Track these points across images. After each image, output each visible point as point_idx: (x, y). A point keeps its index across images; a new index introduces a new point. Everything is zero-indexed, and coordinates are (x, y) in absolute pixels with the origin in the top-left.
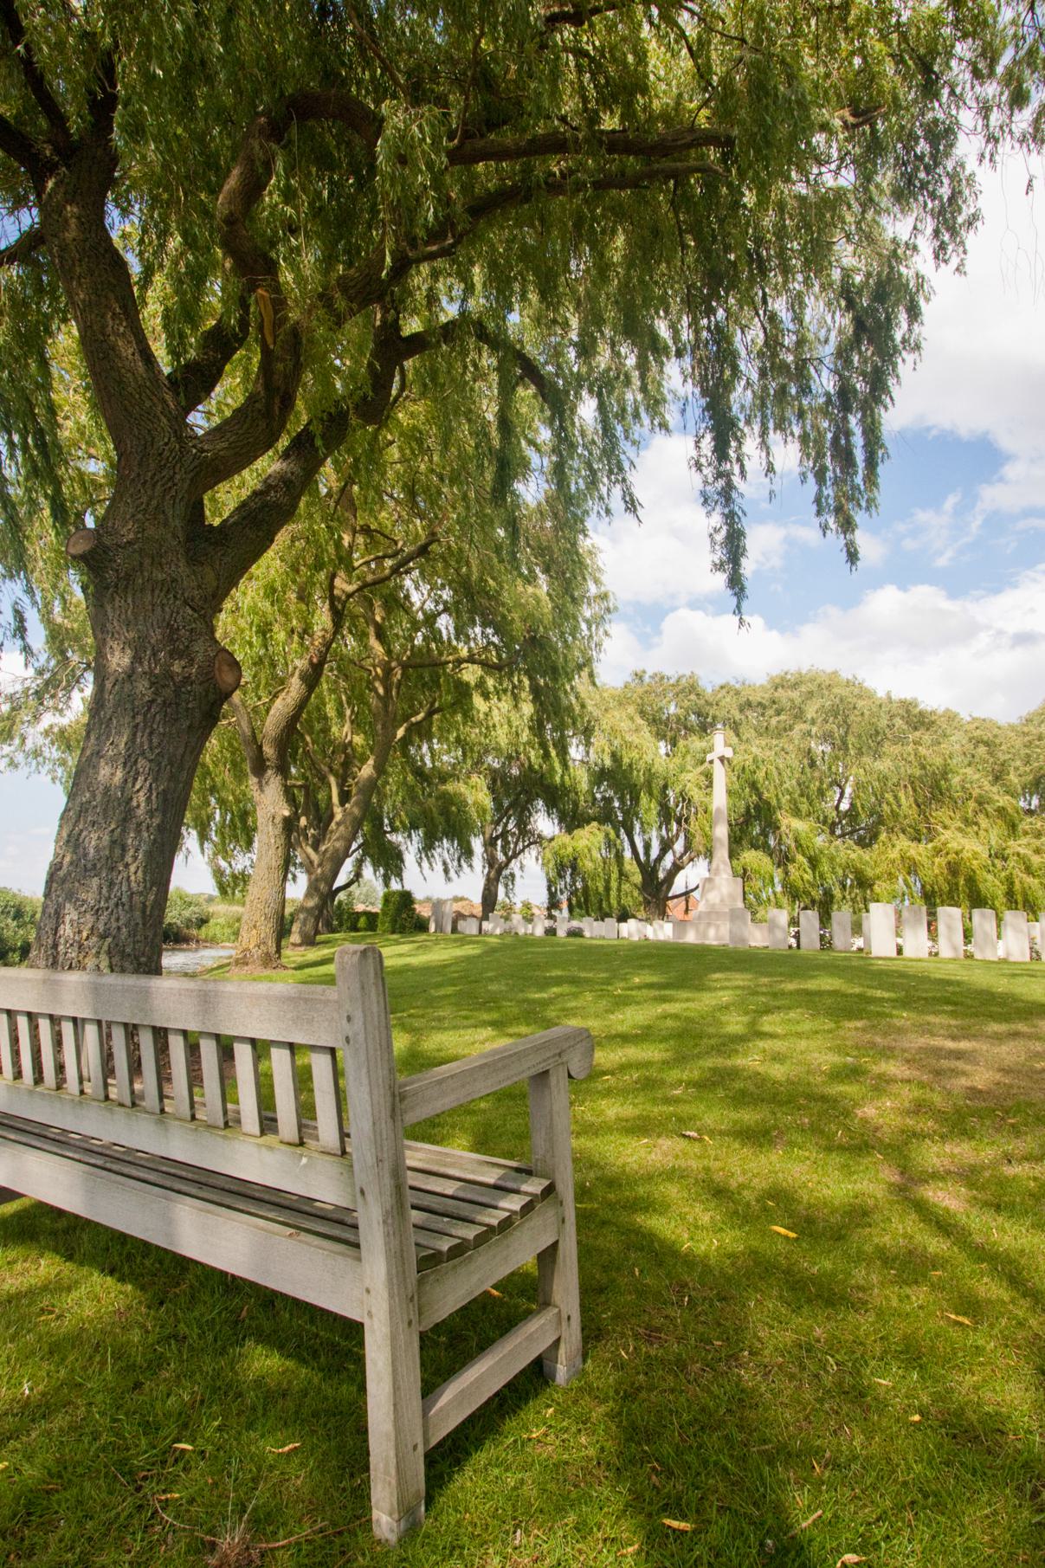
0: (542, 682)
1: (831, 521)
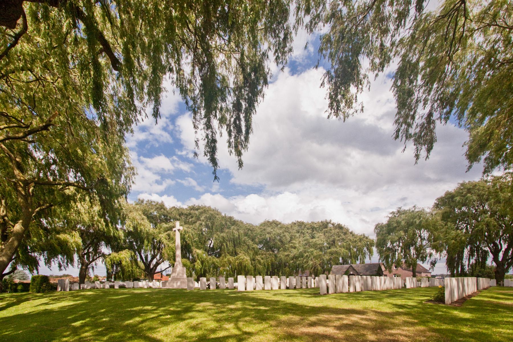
0: (104, 198)
1: (233, 151)
